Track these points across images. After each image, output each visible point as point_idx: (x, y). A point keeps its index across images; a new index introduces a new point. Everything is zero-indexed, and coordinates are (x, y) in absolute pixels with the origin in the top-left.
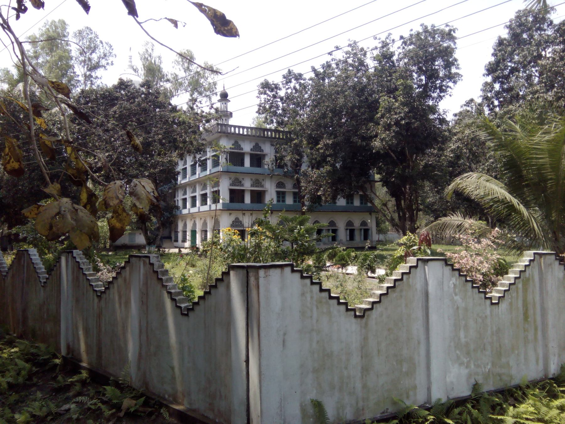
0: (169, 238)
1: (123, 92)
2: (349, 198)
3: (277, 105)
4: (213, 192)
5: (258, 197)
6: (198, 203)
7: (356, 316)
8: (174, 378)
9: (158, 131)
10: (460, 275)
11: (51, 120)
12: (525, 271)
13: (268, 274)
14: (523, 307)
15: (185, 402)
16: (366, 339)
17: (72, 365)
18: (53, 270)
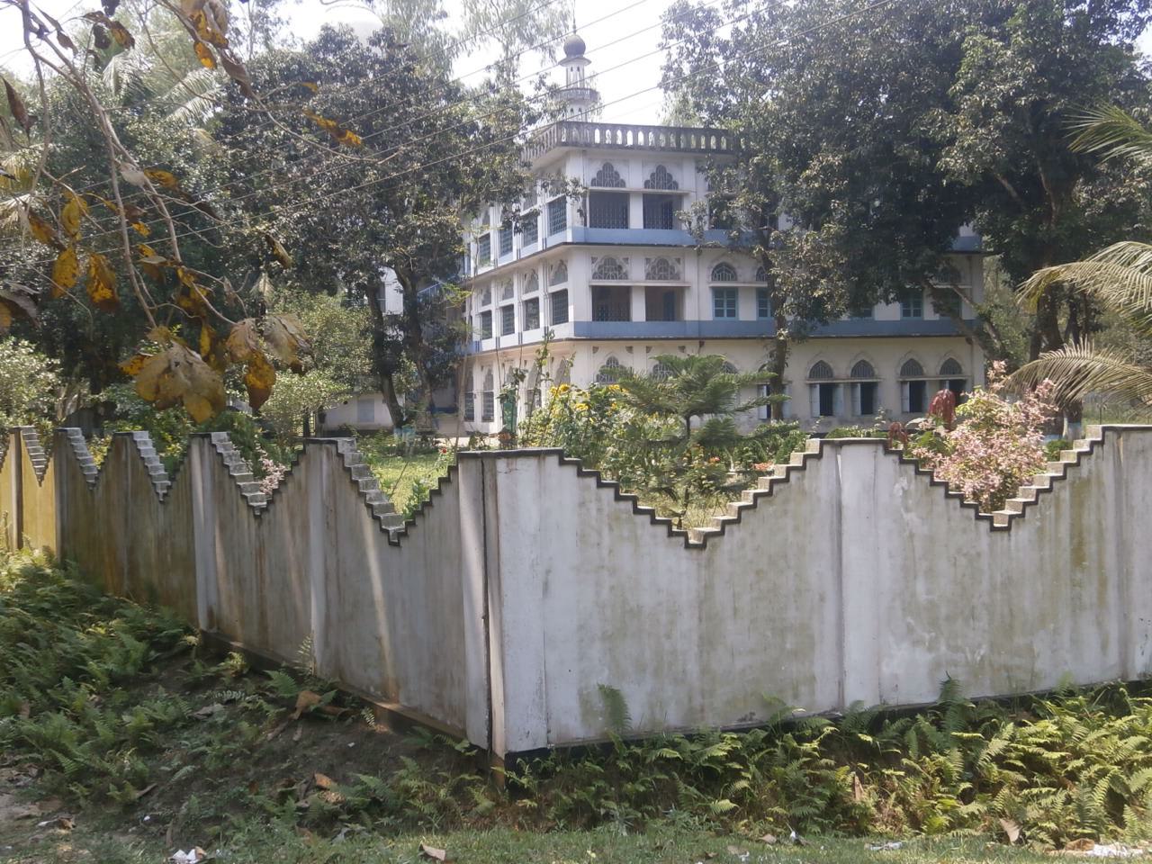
0: (452, 410)
1: (331, 58)
2: (910, 300)
3: (712, 63)
4: (527, 302)
5: (665, 303)
6: (518, 322)
7: (688, 546)
8: (381, 657)
9: (412, 151)
10: (918, 473)
11: (172, 139)
12: (1078, 464)
13: (514, 466)
14: (1072, 538)
15: (402, 698)
16: (709, 587)
17: (216, 647)
18: (178, 470)
